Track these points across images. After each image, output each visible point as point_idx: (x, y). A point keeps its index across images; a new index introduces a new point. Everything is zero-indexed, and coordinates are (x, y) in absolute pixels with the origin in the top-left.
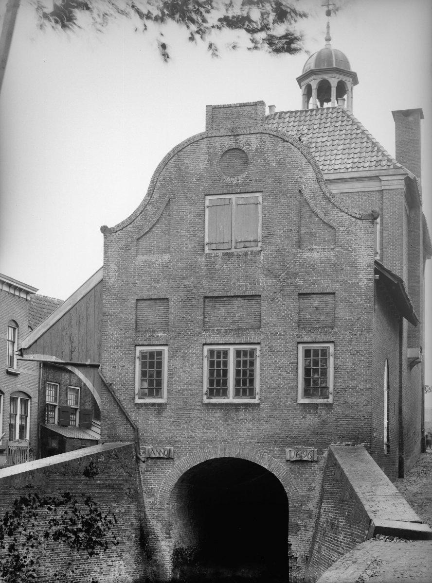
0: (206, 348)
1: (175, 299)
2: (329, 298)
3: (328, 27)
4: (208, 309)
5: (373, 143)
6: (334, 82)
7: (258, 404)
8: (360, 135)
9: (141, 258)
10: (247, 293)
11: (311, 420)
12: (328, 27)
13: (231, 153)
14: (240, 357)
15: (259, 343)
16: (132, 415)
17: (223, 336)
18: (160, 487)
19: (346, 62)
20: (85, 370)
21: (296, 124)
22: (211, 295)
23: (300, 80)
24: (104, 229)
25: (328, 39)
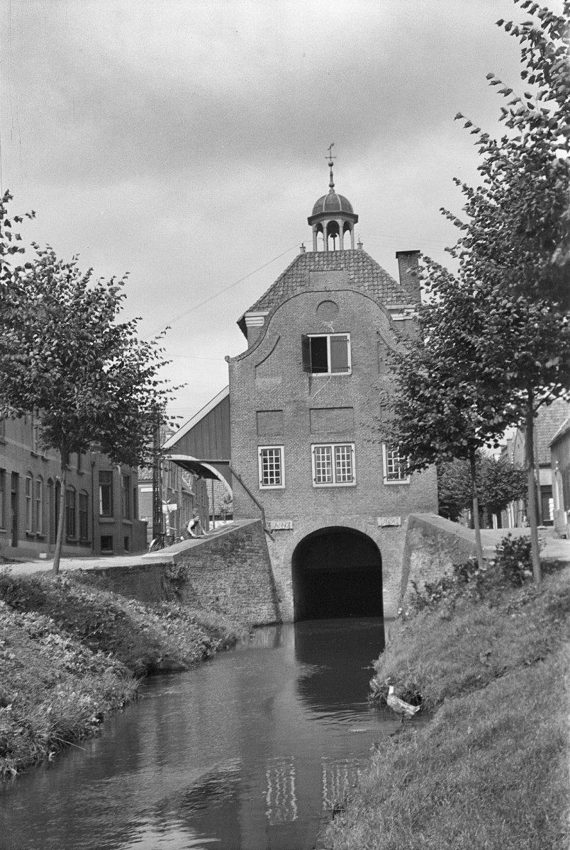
0: (313, 446)
1: (288, 410)
2: (347, 411)
3: (332, 175)
4: (313, 418)
5: (391, 282)
6: (340, 222)
7: (355, 487)
8: (379, 275)
9: (259, 382)
10: (343, 406)
11: (395, 497)
12: (332, 175)
13: (325, 304)
14: (273, 469)
15: (354, 442)
16: (258, 498)
17: (326, 438)
18: (281, 553)
19: (350, 207)
20: (220, 466)
21: (325, 263)
22: (315, 407)
23: (310, 221)
24: (227, 359)
25: (332, 186)
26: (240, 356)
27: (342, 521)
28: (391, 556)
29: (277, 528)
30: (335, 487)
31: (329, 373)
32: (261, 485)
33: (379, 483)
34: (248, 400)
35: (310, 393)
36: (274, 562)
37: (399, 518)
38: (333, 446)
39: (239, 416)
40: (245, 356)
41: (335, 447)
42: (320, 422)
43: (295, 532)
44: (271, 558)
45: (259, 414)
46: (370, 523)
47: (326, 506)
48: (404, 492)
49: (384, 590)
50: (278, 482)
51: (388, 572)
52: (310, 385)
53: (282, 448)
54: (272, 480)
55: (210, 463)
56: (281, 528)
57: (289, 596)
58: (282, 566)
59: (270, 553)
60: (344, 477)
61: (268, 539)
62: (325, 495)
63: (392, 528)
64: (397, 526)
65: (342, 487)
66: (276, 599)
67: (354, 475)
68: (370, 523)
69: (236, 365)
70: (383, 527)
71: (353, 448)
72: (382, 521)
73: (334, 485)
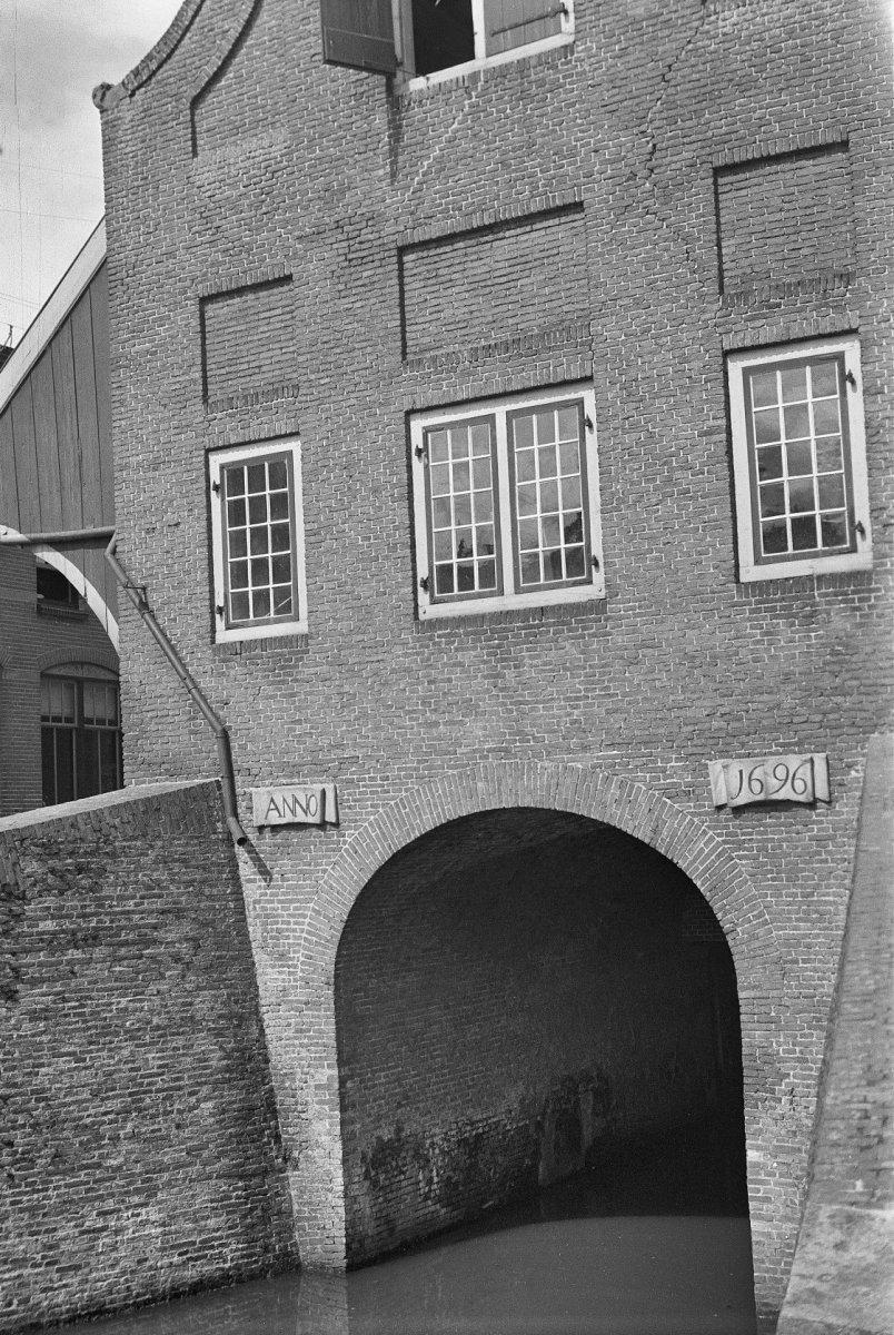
2: (556, 232)
7: (597, 607)
11: (791, 645)
18: (296, 931)
20: (79, 553)
26: (136, 72)
27: (537, 784)
28: (783, 967)
29: (274, 819)
30: (508, 615)
31: (481, 61)
32: (423, 598)
33: (714, 576)
34: (171, 255)
35: (393, 175)
36: (269, 978)
37: (819, 759)
38: (500, 411)
39: (136, 332)
40: (153, 66)
41: (510, 415)
42: (448, 300)
43: (350, 835)
44: (259, 957)
45: (211, 309)
46: (672, 793)
47: (470, 708)
48: (840, 622)
49: (752, 1156)
50: (287, 608)
51: (770, 1058)
52: (396, 136)
53: (294, 446)
54: (804, 529)
55: (58, 544)
56: (288, 818)
57: (324, 1139)
58: (300, 995)
59: (255, 931)
60: (466, 572)
61: (246, 870)
62: (467, 657)
63: (783, 816)
64: (812, 805)
65: (542, 611)
66: (257, 1126)
67: (597, 550)
68: (672, 793)
69: (127, 113)
70: (738, 810)
71: (853, 363)
72: (727, 780)
73: (511, 601)
